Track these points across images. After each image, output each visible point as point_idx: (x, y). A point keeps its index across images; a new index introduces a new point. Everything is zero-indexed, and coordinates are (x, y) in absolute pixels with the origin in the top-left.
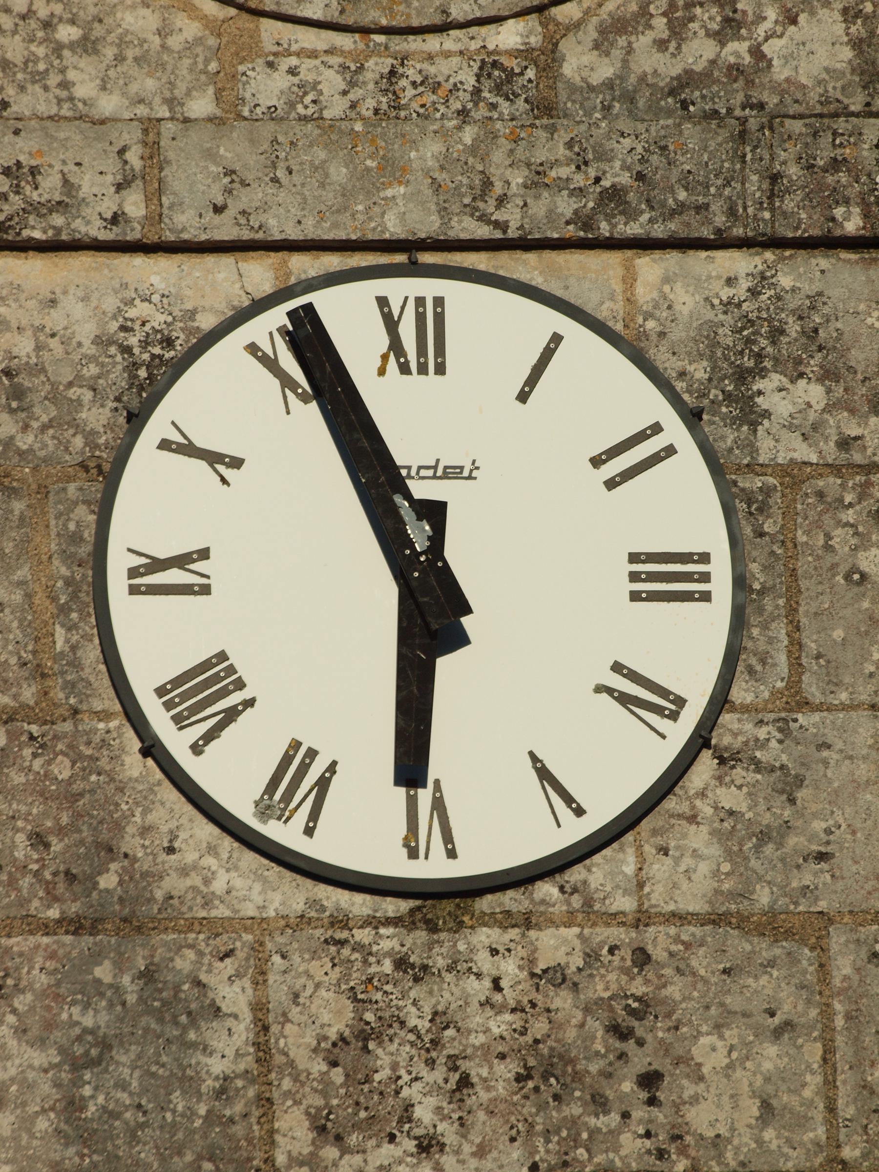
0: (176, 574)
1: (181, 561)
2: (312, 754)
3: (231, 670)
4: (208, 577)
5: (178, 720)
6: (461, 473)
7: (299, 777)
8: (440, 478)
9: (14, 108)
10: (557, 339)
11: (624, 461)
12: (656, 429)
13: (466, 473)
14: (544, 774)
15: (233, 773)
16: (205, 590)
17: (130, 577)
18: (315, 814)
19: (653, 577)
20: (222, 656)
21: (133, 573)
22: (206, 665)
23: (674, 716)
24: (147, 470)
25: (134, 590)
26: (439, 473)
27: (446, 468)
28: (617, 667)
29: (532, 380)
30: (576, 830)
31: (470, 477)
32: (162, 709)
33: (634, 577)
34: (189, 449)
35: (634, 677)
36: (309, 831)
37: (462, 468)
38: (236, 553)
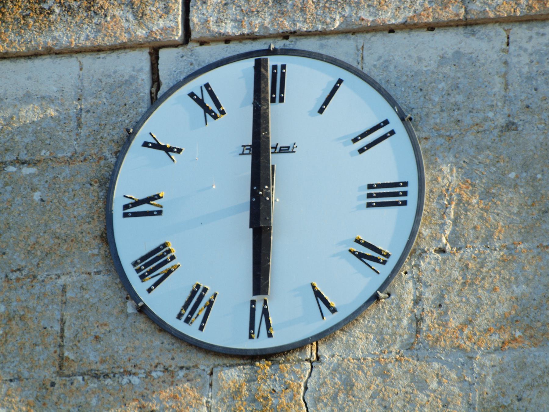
0: (145, 207)
1: (148, 200)
2: (205, 290)
3: (169, 251)
4: (201, 87)
5: (143, 277)
6: (288, 150)
7: (197, 302)
8: (278, 153)
9: (109, 111)
10: (340, 81)
11: (369, 139)
12: (386, 122)
13: (290, 150)
14: (318, 294)
15: (165, 301)
16: (160, 213)
17: (124, 210)
18: (156, 284)
19: (379, 195)
20: (165, 245)
21: (126, 207)
22: (158, 250)
23: (384, 262)
24: (136, 158)
25: (125, 215)
26: (278, 150)
27: (281, 147)
28: (358, 241)
29: (326, 102)
30: (330, 320)
31: (293, 152)
32: (135, 272)
33: (370, 196)
34: (157, 146)
35: (366, 245)
36: (201, 328)
37: (289, 147)
38: (184, 179)
